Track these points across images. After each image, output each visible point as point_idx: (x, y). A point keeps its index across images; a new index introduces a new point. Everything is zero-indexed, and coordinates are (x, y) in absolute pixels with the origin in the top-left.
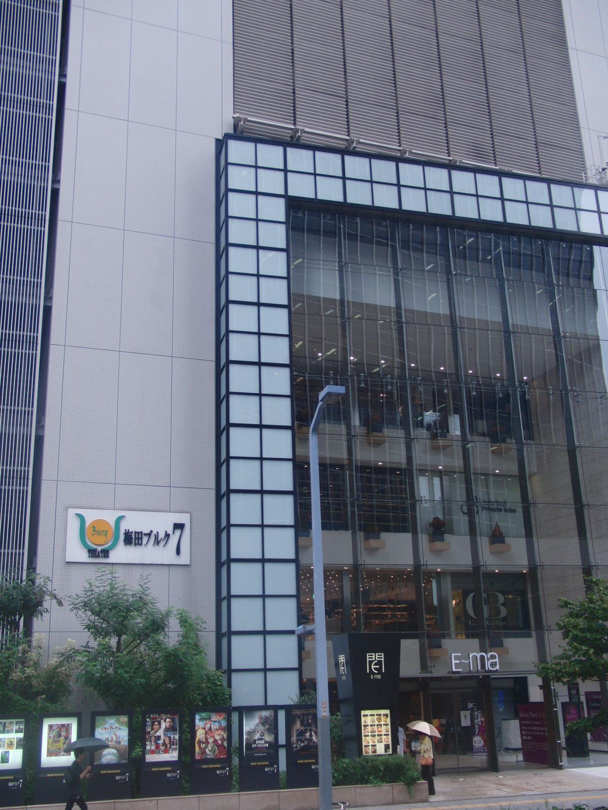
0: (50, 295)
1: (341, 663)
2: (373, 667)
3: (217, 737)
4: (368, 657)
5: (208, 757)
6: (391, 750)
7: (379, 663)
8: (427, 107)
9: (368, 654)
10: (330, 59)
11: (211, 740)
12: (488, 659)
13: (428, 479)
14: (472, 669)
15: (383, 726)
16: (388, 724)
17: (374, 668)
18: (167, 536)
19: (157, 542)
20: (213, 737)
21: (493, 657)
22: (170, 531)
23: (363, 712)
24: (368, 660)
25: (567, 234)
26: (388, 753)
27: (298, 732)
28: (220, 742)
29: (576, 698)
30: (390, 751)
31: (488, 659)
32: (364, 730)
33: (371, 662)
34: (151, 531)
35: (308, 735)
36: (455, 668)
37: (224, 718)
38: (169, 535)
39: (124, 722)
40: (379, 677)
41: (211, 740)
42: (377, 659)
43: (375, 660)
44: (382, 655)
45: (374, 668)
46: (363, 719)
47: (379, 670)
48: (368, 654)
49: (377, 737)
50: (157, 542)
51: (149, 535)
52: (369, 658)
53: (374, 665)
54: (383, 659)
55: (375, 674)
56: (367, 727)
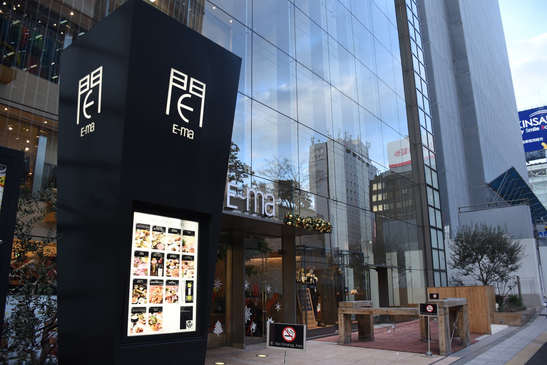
0: (404, 254)
2: (180, 105)
6: (194, 321)
7: (194, 101)
12: (189, 133)
13: (345, 285)
14: (387, 209)
15: (148, 285)
16: (192, 258)
21: (191, 133)
23: (139, 218)
24: (171, 83)
26: (188, 330)
30: (193, 326)
31: (189, 133)
32: (136, 266)
33: (177, 93)
35: (25, 249)
36: (231, 204)
40: (190, 134)
42: (191, 91)
43: (187, 92)
46: (136, 234)
47: (193, 117)
49: (164, 286)
53: (184, 102)
54: (203, 97)
55: (181, 123)
56: (144, 259)
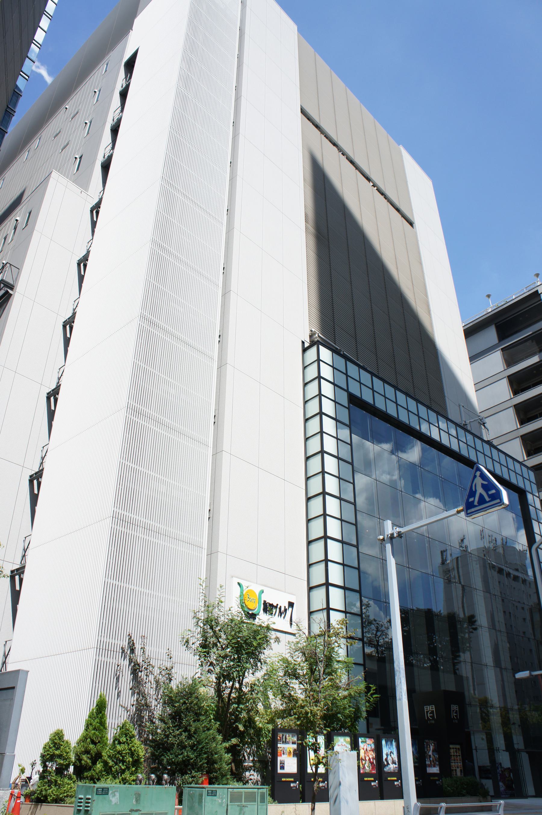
1: (453, 711)
2: (429, 715)
3: (371, 757)
4: (425, 708)
5: (367, 771)
7: (432, 712)
8: (329, 331)
9: (452, 705)
10: (362, 360)
11: (367, 758)
17: (430, 716)
18: (286, 610)
19: (281, 613)
20: (369, 756)
22: (287, 607)
24: (425, 710)
25: (393, 418)
27: (37, 804)
28: (372, 760)
29: (312, 769)
33: (427, 712)
34: (277, 605)
37: (373, 742)
38: (286, 609)
39: (348, 742)
40: (433, 722)
41: (367, 758)
42: (431, 709)
44: (433, 707)
45: (430, 716)
47: (433, 717)
48: (425, 707)
50: (281, 613)
51: (276, 607)
52: (426, 709)
53: (430, 714)
54: (434, 710)
